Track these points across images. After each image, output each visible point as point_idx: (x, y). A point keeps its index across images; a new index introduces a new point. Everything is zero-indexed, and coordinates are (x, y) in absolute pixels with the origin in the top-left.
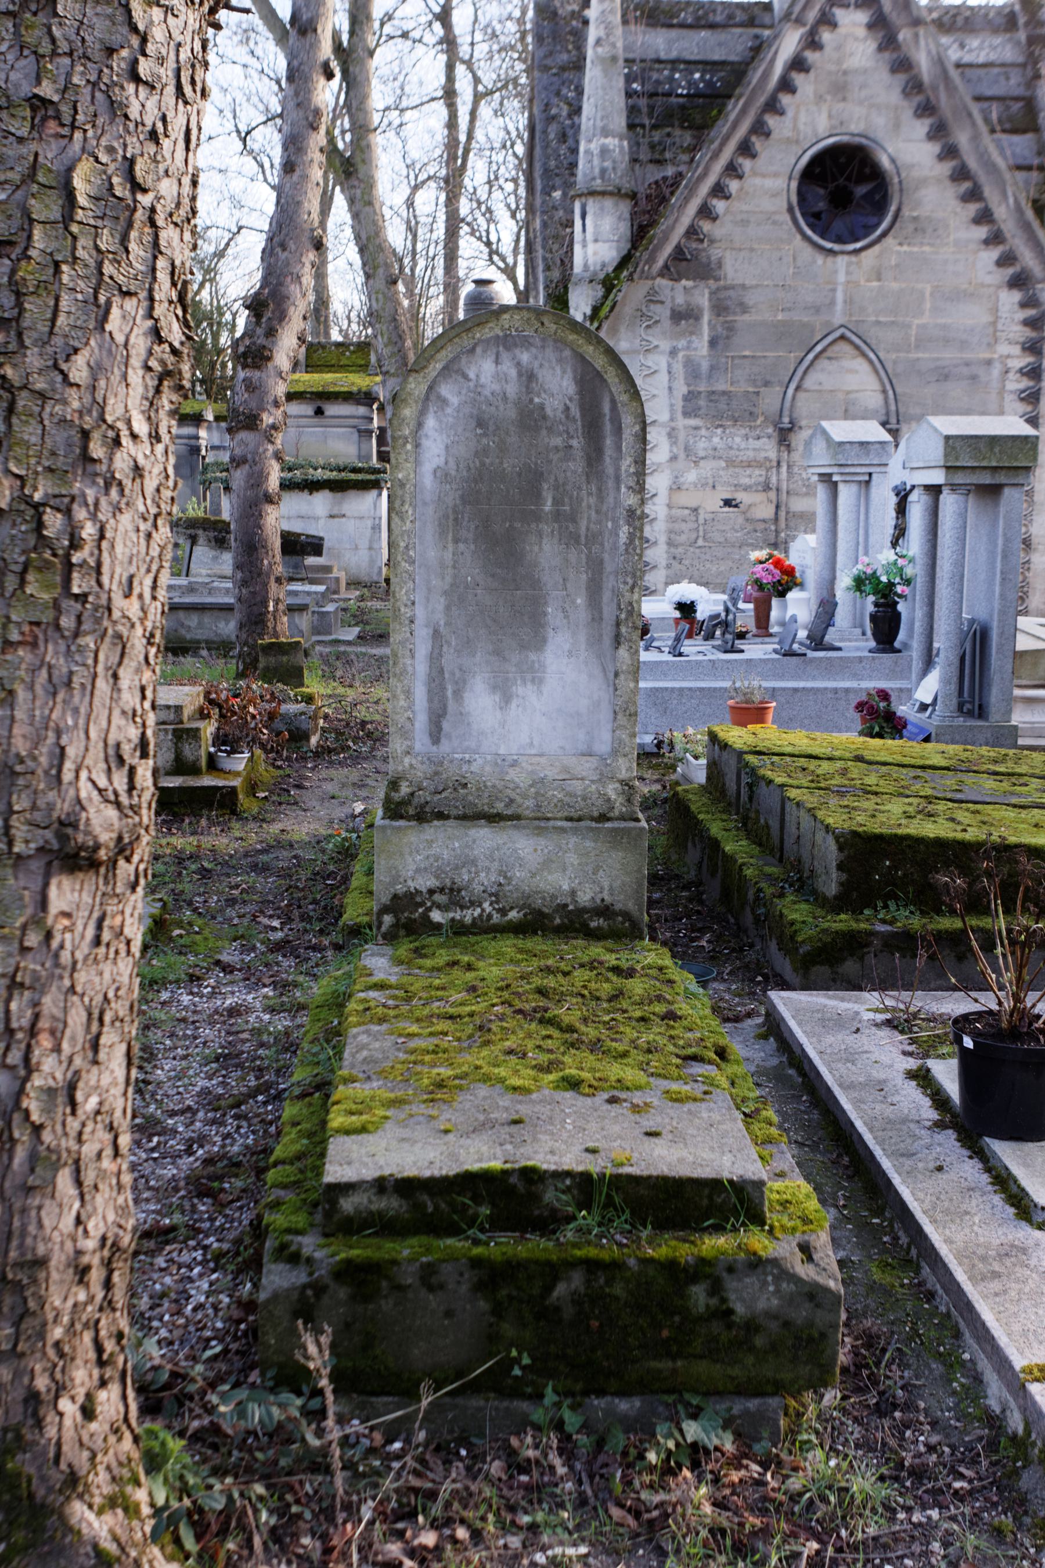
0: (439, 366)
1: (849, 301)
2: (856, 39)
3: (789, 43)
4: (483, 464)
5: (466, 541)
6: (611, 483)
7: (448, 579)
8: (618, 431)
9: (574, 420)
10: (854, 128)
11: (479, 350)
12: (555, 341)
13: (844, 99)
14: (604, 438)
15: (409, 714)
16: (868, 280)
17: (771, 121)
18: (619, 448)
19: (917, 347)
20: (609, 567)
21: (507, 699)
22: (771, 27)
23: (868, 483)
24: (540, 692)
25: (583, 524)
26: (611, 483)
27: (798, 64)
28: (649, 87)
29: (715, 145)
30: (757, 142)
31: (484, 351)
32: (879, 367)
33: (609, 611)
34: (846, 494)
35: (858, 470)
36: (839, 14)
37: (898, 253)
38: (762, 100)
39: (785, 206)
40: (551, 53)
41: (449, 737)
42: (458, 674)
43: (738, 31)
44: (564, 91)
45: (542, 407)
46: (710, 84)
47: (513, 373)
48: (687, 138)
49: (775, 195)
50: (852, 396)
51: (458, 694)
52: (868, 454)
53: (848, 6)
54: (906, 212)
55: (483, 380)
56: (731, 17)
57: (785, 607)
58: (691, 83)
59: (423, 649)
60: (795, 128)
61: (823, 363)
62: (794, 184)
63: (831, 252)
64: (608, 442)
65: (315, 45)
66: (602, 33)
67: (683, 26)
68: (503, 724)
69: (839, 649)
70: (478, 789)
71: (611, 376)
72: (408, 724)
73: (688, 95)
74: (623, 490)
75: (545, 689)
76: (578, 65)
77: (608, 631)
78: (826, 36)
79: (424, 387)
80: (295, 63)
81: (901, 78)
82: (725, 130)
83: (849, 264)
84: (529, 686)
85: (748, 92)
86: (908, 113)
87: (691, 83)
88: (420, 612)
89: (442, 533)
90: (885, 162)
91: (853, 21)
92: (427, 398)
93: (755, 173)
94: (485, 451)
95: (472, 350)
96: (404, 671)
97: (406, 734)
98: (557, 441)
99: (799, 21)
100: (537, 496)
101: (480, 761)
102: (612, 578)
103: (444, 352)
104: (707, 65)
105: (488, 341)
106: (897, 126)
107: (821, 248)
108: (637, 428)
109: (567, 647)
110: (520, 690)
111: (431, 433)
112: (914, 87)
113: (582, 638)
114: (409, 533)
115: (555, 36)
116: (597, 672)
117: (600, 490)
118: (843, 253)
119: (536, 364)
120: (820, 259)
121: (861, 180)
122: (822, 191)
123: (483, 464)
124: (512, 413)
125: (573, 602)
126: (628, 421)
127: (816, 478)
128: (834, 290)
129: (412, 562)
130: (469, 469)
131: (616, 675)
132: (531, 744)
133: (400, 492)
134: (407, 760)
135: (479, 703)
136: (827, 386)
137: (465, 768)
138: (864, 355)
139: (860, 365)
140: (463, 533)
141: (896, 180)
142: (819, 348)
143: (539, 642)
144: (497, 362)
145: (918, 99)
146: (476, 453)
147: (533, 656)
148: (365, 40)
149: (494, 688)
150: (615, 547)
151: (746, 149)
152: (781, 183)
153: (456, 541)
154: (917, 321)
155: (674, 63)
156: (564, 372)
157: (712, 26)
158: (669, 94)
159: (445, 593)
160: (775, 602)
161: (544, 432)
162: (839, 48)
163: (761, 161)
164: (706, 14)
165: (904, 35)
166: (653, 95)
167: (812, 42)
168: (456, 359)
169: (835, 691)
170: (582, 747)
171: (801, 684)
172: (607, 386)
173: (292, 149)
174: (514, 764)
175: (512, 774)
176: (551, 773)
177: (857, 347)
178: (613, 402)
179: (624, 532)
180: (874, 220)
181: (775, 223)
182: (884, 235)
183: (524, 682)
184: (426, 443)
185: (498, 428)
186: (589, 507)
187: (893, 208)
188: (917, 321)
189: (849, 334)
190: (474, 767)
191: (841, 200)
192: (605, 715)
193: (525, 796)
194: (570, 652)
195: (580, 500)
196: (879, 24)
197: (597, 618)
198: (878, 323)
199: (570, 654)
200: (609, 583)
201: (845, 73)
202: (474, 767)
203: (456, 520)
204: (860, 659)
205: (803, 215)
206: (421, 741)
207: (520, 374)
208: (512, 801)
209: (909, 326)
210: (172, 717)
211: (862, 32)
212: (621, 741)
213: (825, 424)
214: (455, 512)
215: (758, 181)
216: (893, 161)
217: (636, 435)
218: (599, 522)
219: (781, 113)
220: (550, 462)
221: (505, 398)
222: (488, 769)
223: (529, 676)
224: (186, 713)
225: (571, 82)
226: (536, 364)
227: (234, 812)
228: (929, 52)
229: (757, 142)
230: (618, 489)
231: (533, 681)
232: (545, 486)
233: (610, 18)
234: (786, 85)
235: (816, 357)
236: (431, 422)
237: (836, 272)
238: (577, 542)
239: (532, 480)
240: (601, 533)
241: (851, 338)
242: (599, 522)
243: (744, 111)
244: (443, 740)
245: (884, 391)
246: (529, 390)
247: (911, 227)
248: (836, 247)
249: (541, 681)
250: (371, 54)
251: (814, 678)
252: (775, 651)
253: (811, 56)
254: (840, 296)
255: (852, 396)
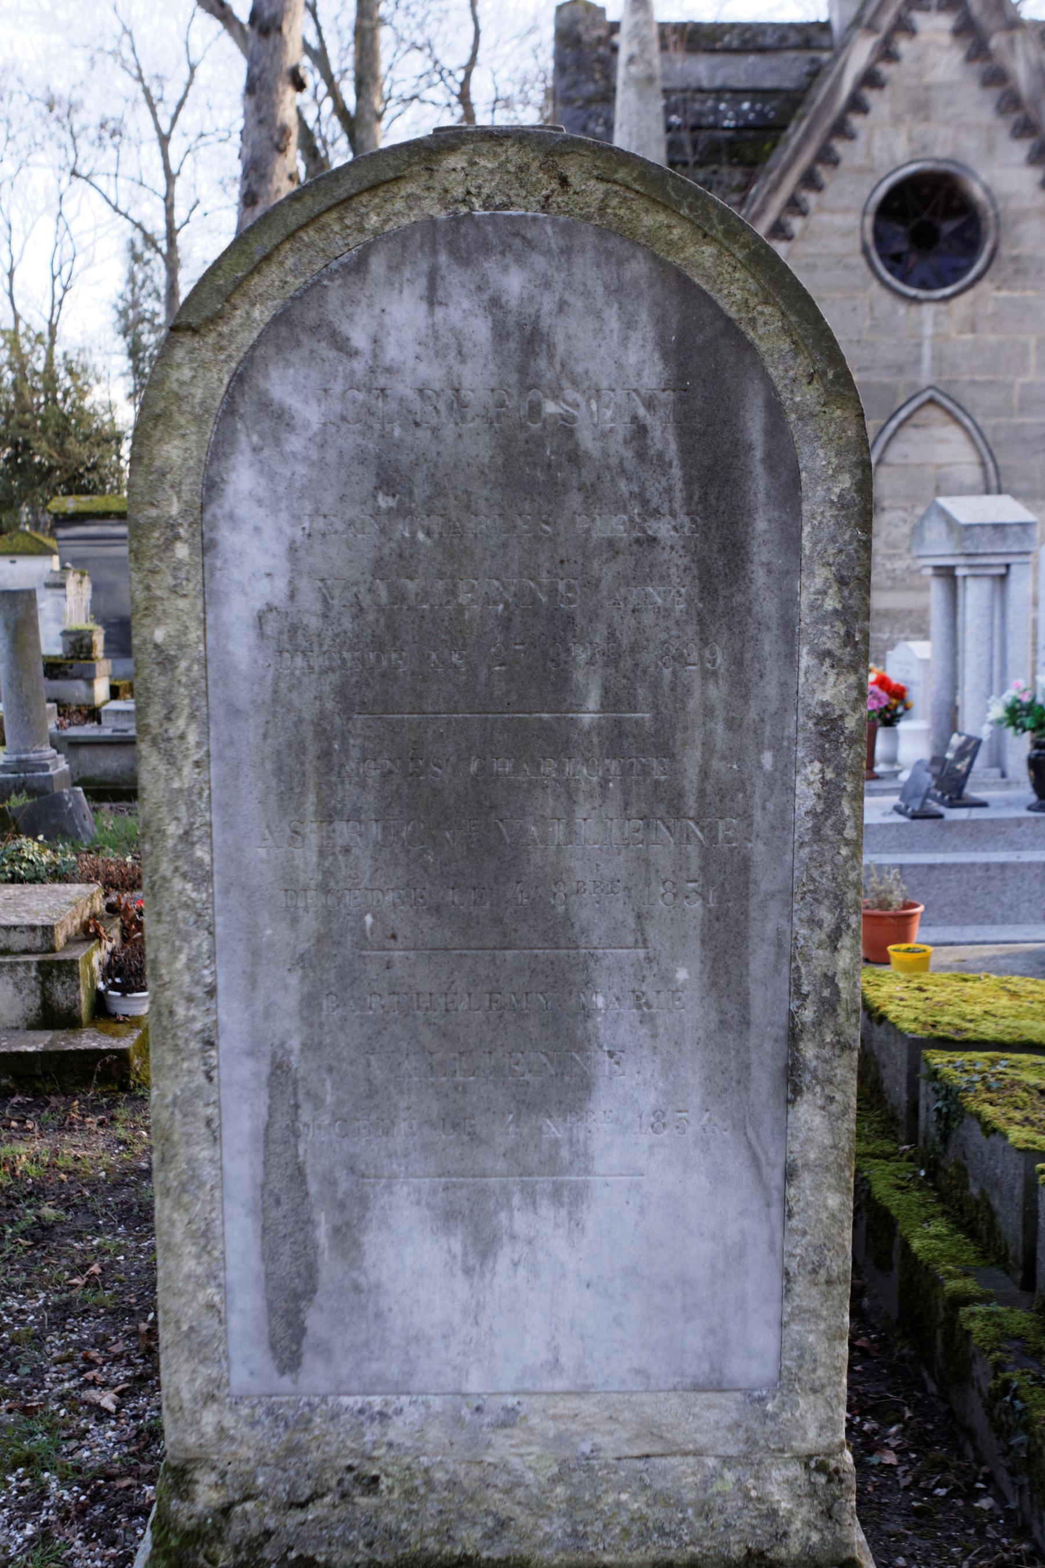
0: (262, 314)
1: (938, 358)
2: (939, 48)
3: (860, 54)
4: (398, 596)
5: (355, 815)
6: (769, 643)
7: (310, 923)
8: (790, 492)
9: (662, 464)
10: (939, 152)
11: (377, 264)
12: (602, 233)
13: (927, 119)
14: (750, 513)
15: (211, 1293)
16: (961, 332)
17: (840, 147)
18: (792, 542)
19: (1022, 410)
20: (767, 879)
21: (484, 1245)
22: (830, 48)
23: (1003, 578)
24: (577, 1225)
25: (692, 760)
26: (769, 643)
27: (870, 79)
28: (691, 121)
29: (774, 176)
30: (823, 173)
31: (394, 268)
32: (976, 436)
33: (767, 1002)
34: (975, 595)
35: (992, 560)
36: (919, 19)
37: (996, 299)
38: (828, 121)
39: (858, 246)
40: (574, 85)
41: (325, 1351)
42: (344, 1184)
43: (791, 55)
44: (591, 125)
45: (566, 427)
46: (761, 114)
47: (480, 329)
48: (737, 176)
49: (846, 234)
50: (946, 470)
51: (346, 1236)
52: (1004, 539)
53: (928, 9)
54: (1004, 251)
55: (391, 353)
56: (783, 39)
57: (895, 739)
58: (739, 114)
59: (242, 1117)
60: (869, 154)
61: (908, 432)
62: (869, 221)
63: (915, 300)
64: (761, 525)
65: (280, 48)
66: (635, 49)
67: (728, 50)
68: (474, 1313)
69: (983, 805)
70: (409, 1493)
71: (769, 333)
72: (211, 1323)
73: (736, 128)
74: (806, 660)
75: (593, 1217)
76: (608, 96)
77: (765, 1055)
78: (903, 45)
79: (220, 378)
80: (256, 70)
81: (995, 92)
82: (785, 157)
83: (937, 314)
84: (545, 1208)
85: (812, 111)
86: (1003, 133)
87: (739, 114)
88: (232, 1017)
89: (287, 789)
90: (977, 192)
91: (935, 26)
92: (230, 410)
93: (821, 209)
94: (405, 559)
95: (359, 266)
96: (191, 1181)
97: (202, 1348)
98: (613, 526)
99: (871, 28)
100: (558, 684)
101: (413, 1414)
102: (775, 908)
103: (273, 274)
104: (756, 93)
105: (402, 237)
106: (991, 150)
107: (903, 296)
108: (846, 481)
109: (649, 1100)
110: (521, 1222)
111: (245, 510)
112: (1010, 102)
113: (692, 1075)
114: (190, 797)
115: (580, 65)
116: (736, 1166)
117: (738, 662)
118: (929, 300)
119: (547, 303)
120: (902, 309)
121: (949, 213)
122: (901, 229)
123: (398, 596)
124: (479, 448)
125: (667, 978)
126: (819, 463)
127: (929, 571)
128: (919, 345)
129: (203, 878)
130: (359, 611)
131: (790, 1174)
132: (554, 1366)
133: (160, 683)
134: (209, 1419)
135: (408, 1256)
136: (915, 457)
137: (371, 1433)
138: (957, 421)
139: (954, 433)
140: (349, 794)
141: (991, 213)
142: (903, 414)
143: (573, 1092)
144: (432, 299)
145: (1015, 117)
146: (379, 567)
147: (553, 1129)
148: (371, 103)
149: (448, 1217)
150: (783, 823)
151: (810, 181)
152: (852, 220)
153: (328, 816)
154: (1021, 380)
155: (719, 93)
156: (629, 324)
157: (762, 50)
158: (714, 127)
159: (301, 959)
160: (881, 734)
161: (575, 500)
162: (919, 58)
163: (829, 195)
164: (755, 36)
165: (997, 42)
166: (696, 128)
167: (887, 53)
168: (313, 289)
169: (987, 866)
170: (697, 1369)
171: (938, 858)
172: (757, 361)
173: (253, 176)
174: (509, 1419)
175: (503, 1447)
176: (611, 1443)
177: (949, 412)
178: (775, 408)
179: (808, 782)
180: (963, 262)
181: (847, 267)
182: (979, 277)
183: (531, 1197)
184: (230, 539)
185: (440, 492)
186: (708, 711)
187: (988, 247)
188: (1021, 380)
189: (939, 397)
190: (397, 1431)
191: (924, 239)
192: (759, 1280)
193: (539, 1508)
194: (658, 1114)
195: (680, 691)
196: (967, 29)
197: (733, 1019)
198: (973, 383)
199: (659, 1120)
200: (767, 923)
201: (927, 88)
202: (397, 1431)
203: (325, 755)
204: (1019, 822)
205: (882, 257)
206: (248, 1364)
207: (500, 334)
208: (503, 1524)
209: (1011, 386)
210: (38, 942)
211: (946, 39)
212: (803, 1352)
213: (942, 501)
214: (321, 734)
215: (825, 218)
216: (987, 190)
217: (842, 503)
218: (737, 754)
219: (851, 136)
220: (593, 585)
221: (458, 404)
222: (435, 1433)
223: (544, 1183)
224: (60, 938)
225: (599, 116)
226: (547, 303)
227: (124, 1088)
228: (1028, 61)
229: (823, 173)
230: (791, 658)
231: (556, 1194)
232: (581, 655)
233: (645, 31)
234: (857, 104)
235: (901, 425)
236: (243, 479)
237: (921, 323)
238: (676, 811)
239: (542, 640)
240: (742, 785)
241: (943, 403)
242: (737, 754)
243: (807, 136)
244: (308, 1359)
245: (983, 464)
246: (528, 380)
247: (1010, 268)
248: (922, 294)
249: (579, 1195)
250: (379, 117)
251: (955, 849)
252: (897, 809)
253: (886, 69)
254: (927, 352)
255: (946, 470)
